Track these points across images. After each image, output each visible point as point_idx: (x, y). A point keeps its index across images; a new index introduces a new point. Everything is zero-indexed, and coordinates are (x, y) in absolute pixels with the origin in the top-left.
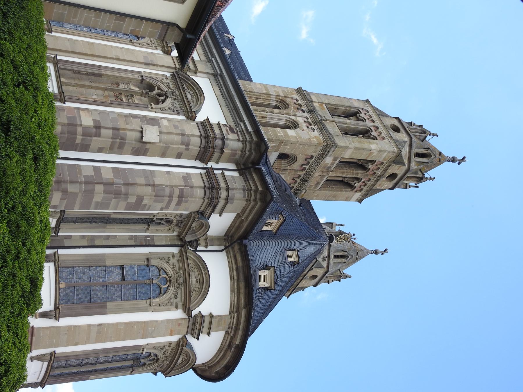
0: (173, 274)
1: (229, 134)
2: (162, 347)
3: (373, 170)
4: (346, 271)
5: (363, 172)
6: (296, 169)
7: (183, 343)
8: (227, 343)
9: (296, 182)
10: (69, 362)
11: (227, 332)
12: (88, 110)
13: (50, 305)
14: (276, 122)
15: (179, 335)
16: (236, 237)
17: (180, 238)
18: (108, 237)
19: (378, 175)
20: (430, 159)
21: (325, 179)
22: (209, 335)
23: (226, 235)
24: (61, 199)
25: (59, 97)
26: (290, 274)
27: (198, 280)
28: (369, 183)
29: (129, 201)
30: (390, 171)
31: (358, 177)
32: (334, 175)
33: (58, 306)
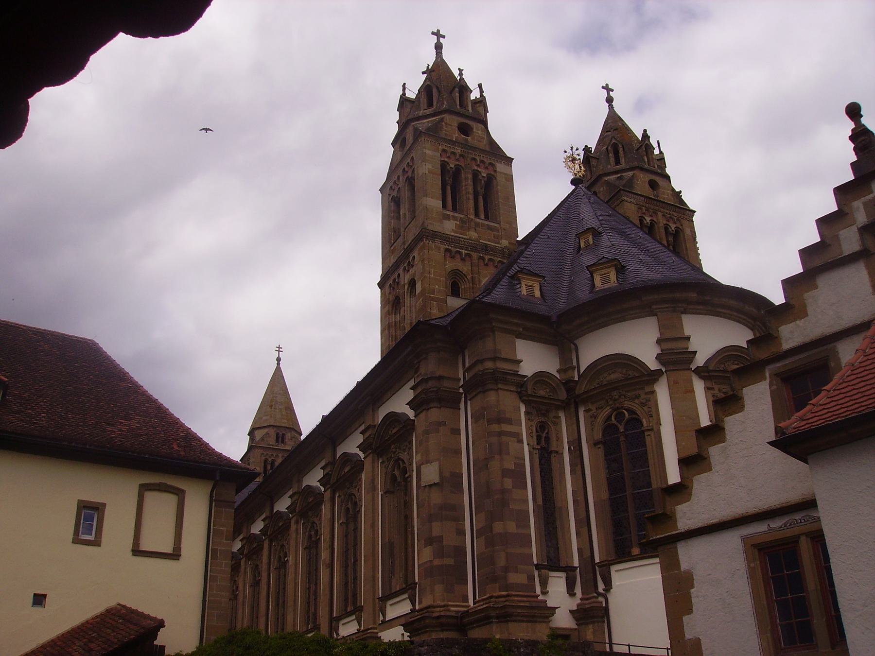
0: (608, 408)
1: (421, 374)
8: (701, 307)
9: (490, 260)
11: (683, 313)
15: (692, 379)
17: (565, 406)
19: (463, 150)
20: (432, 85)
24: (517, 572)
27: (613, 371)
29: (510, 487)
30: (456, 135)
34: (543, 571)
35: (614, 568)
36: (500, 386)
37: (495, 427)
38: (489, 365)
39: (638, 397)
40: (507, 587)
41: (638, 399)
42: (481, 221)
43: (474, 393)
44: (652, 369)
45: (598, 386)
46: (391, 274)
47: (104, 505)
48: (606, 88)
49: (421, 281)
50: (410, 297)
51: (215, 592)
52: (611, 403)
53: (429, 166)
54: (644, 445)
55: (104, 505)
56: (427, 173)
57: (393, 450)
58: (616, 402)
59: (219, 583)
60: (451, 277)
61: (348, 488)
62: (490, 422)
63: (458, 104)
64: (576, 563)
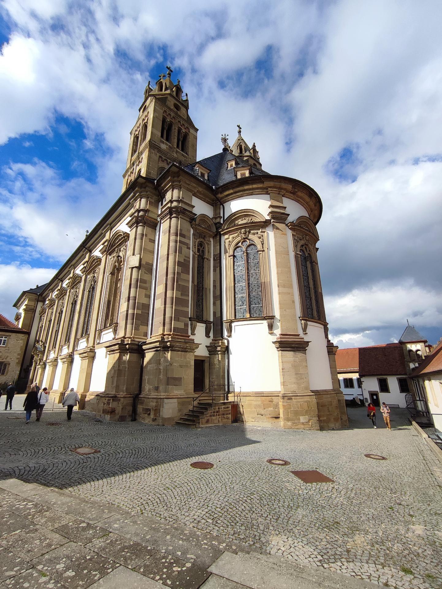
3: (171, 118)
4: (251, 146)
7: (294, 227)
8: (292, 195)
16: (213, 197)
18: (215, 286)
23: (212, 204)
42: (179, 151)
48: (238, 126)
64: (212, 320)
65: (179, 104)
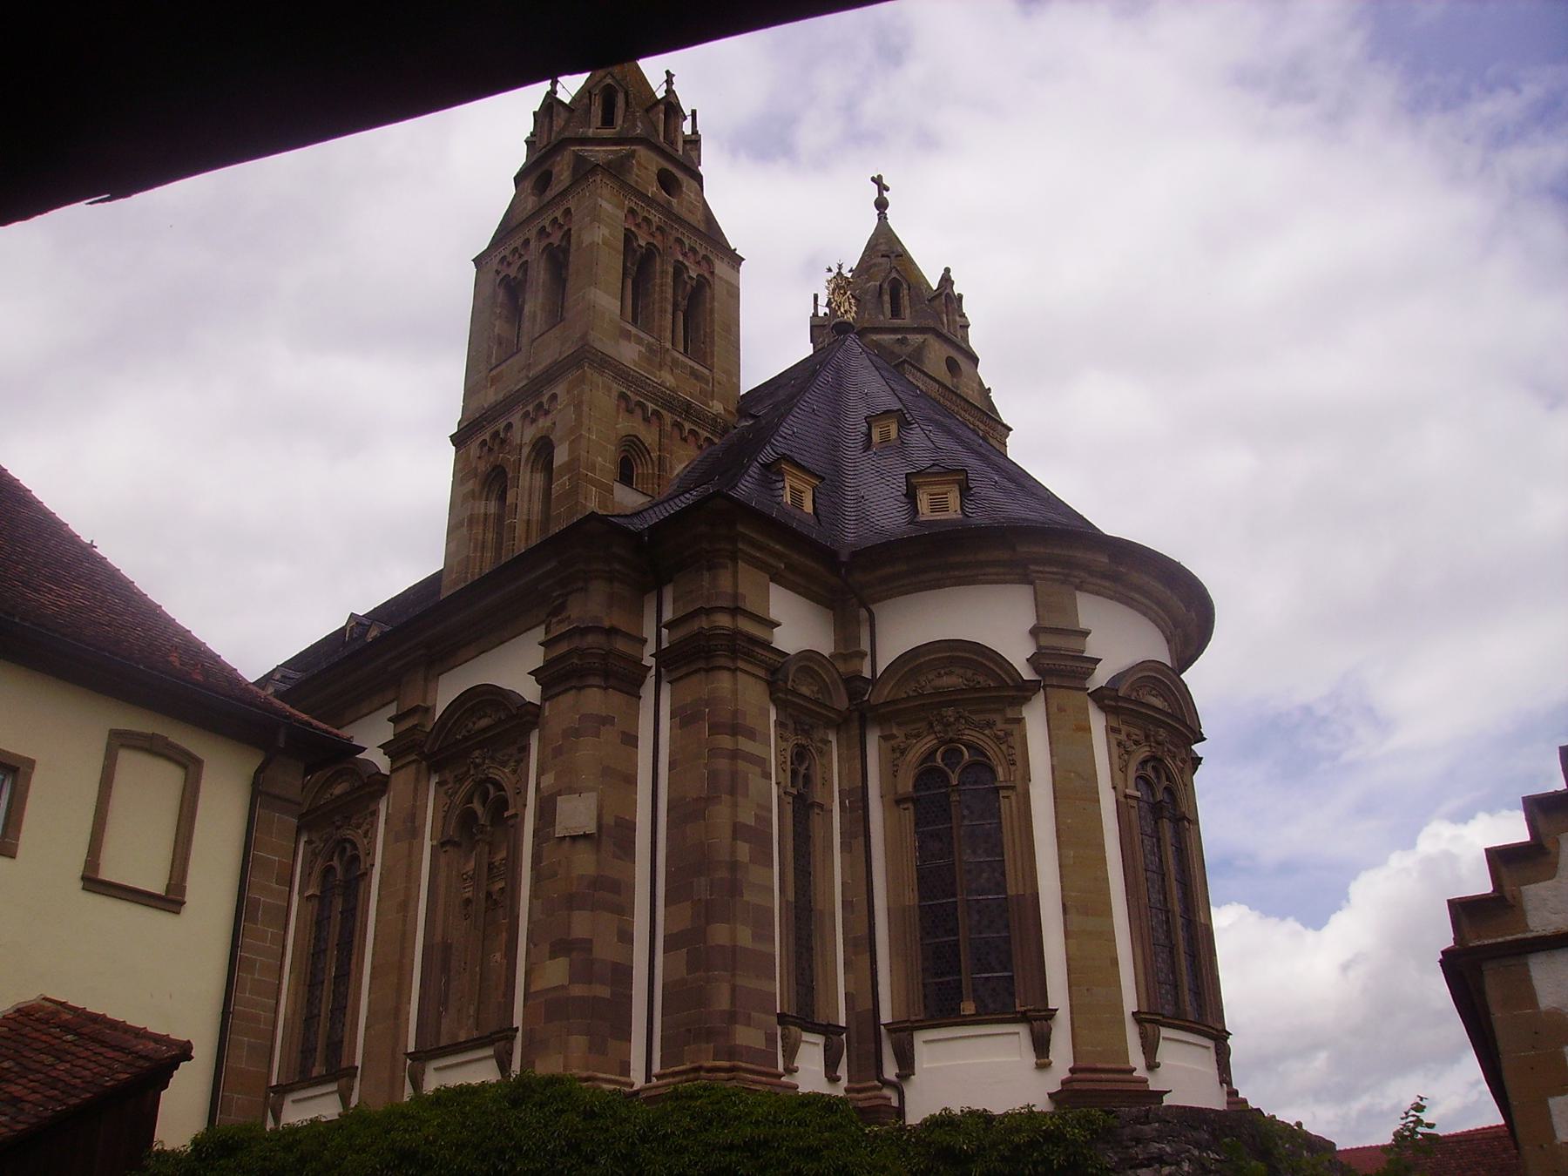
0: (933, 736)
2: (1121, 751)
5: (658, 259)
6: (658, 436)
8: (1107, 584)
10: (1162, 976)
11: (1079, 588)
12: (527, 974)
13: (1018, 1033)
14: (537, 496)
19: (663, 219)
21: (681, 358)
22: (1086, 634)
24: (749, 1025)
25: (503, 1043)
26: (930, 431)
27: (947, 670)
28: (687, 242)
30: (653, 189)
31: (671, 270)
32: (668, 334)
33: (1018, 1016)
34: (792, 1028)
35: (920, 1038)
36: (740, 664)
37: (725, 741)
38: (724, 620)
39: (990, 725)
40: (732, 1053)
41: (991, 728)
43: (684, 671)
44: (1025, 678)
45: (915, 694)
46: (489, 423)
47: (31, 763)
48: (878, 180)
49: (570, 443)
50: (532, 472)
51: (247, 995)
52: (938, 728)
53: (604, 231)
54: (997, 814)
55: (31, 763)
56: (601, 243)
57: (477, 760)
58: (949, 729)
59: (256, 976)
60: (623, 448)
61: (338, 828)
62: (715, 729)
63: (662, 134)
64: (842, 1023)
65: (674, 170)
